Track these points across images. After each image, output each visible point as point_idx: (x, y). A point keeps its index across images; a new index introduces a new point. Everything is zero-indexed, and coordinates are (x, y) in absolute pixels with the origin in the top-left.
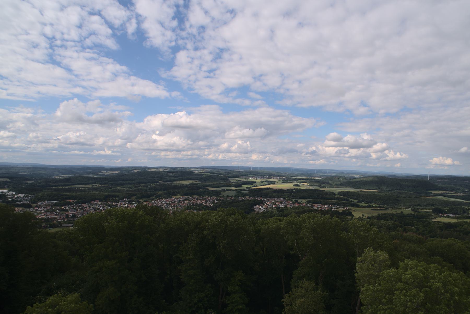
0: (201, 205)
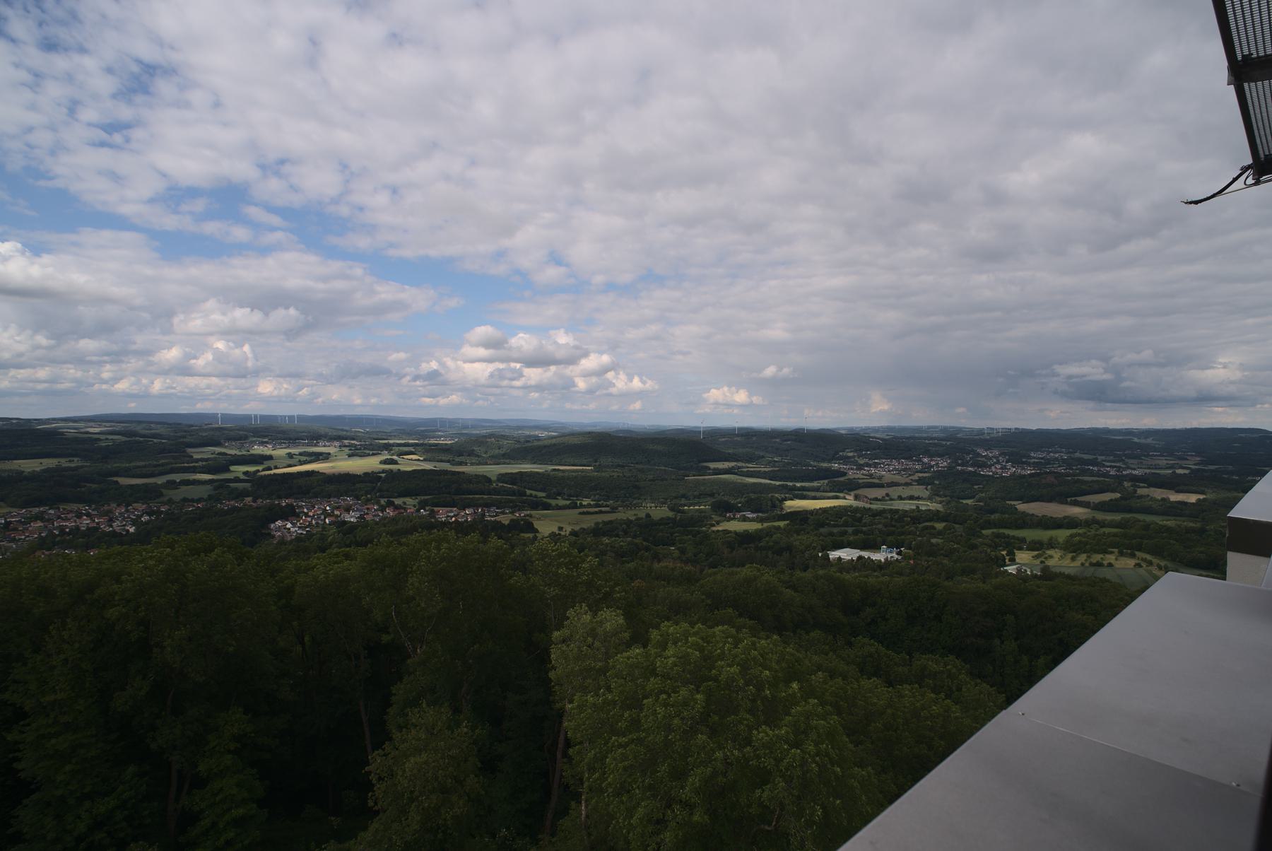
0: (92, 531)
